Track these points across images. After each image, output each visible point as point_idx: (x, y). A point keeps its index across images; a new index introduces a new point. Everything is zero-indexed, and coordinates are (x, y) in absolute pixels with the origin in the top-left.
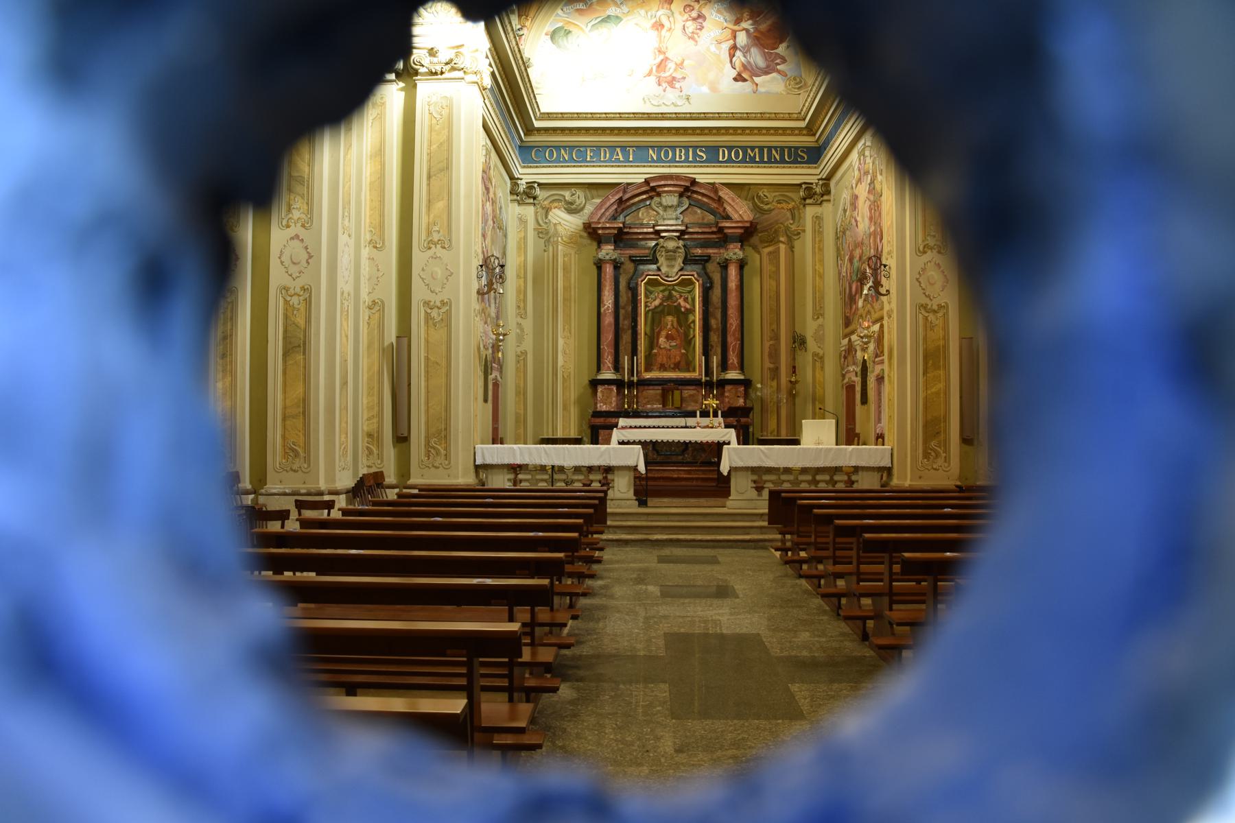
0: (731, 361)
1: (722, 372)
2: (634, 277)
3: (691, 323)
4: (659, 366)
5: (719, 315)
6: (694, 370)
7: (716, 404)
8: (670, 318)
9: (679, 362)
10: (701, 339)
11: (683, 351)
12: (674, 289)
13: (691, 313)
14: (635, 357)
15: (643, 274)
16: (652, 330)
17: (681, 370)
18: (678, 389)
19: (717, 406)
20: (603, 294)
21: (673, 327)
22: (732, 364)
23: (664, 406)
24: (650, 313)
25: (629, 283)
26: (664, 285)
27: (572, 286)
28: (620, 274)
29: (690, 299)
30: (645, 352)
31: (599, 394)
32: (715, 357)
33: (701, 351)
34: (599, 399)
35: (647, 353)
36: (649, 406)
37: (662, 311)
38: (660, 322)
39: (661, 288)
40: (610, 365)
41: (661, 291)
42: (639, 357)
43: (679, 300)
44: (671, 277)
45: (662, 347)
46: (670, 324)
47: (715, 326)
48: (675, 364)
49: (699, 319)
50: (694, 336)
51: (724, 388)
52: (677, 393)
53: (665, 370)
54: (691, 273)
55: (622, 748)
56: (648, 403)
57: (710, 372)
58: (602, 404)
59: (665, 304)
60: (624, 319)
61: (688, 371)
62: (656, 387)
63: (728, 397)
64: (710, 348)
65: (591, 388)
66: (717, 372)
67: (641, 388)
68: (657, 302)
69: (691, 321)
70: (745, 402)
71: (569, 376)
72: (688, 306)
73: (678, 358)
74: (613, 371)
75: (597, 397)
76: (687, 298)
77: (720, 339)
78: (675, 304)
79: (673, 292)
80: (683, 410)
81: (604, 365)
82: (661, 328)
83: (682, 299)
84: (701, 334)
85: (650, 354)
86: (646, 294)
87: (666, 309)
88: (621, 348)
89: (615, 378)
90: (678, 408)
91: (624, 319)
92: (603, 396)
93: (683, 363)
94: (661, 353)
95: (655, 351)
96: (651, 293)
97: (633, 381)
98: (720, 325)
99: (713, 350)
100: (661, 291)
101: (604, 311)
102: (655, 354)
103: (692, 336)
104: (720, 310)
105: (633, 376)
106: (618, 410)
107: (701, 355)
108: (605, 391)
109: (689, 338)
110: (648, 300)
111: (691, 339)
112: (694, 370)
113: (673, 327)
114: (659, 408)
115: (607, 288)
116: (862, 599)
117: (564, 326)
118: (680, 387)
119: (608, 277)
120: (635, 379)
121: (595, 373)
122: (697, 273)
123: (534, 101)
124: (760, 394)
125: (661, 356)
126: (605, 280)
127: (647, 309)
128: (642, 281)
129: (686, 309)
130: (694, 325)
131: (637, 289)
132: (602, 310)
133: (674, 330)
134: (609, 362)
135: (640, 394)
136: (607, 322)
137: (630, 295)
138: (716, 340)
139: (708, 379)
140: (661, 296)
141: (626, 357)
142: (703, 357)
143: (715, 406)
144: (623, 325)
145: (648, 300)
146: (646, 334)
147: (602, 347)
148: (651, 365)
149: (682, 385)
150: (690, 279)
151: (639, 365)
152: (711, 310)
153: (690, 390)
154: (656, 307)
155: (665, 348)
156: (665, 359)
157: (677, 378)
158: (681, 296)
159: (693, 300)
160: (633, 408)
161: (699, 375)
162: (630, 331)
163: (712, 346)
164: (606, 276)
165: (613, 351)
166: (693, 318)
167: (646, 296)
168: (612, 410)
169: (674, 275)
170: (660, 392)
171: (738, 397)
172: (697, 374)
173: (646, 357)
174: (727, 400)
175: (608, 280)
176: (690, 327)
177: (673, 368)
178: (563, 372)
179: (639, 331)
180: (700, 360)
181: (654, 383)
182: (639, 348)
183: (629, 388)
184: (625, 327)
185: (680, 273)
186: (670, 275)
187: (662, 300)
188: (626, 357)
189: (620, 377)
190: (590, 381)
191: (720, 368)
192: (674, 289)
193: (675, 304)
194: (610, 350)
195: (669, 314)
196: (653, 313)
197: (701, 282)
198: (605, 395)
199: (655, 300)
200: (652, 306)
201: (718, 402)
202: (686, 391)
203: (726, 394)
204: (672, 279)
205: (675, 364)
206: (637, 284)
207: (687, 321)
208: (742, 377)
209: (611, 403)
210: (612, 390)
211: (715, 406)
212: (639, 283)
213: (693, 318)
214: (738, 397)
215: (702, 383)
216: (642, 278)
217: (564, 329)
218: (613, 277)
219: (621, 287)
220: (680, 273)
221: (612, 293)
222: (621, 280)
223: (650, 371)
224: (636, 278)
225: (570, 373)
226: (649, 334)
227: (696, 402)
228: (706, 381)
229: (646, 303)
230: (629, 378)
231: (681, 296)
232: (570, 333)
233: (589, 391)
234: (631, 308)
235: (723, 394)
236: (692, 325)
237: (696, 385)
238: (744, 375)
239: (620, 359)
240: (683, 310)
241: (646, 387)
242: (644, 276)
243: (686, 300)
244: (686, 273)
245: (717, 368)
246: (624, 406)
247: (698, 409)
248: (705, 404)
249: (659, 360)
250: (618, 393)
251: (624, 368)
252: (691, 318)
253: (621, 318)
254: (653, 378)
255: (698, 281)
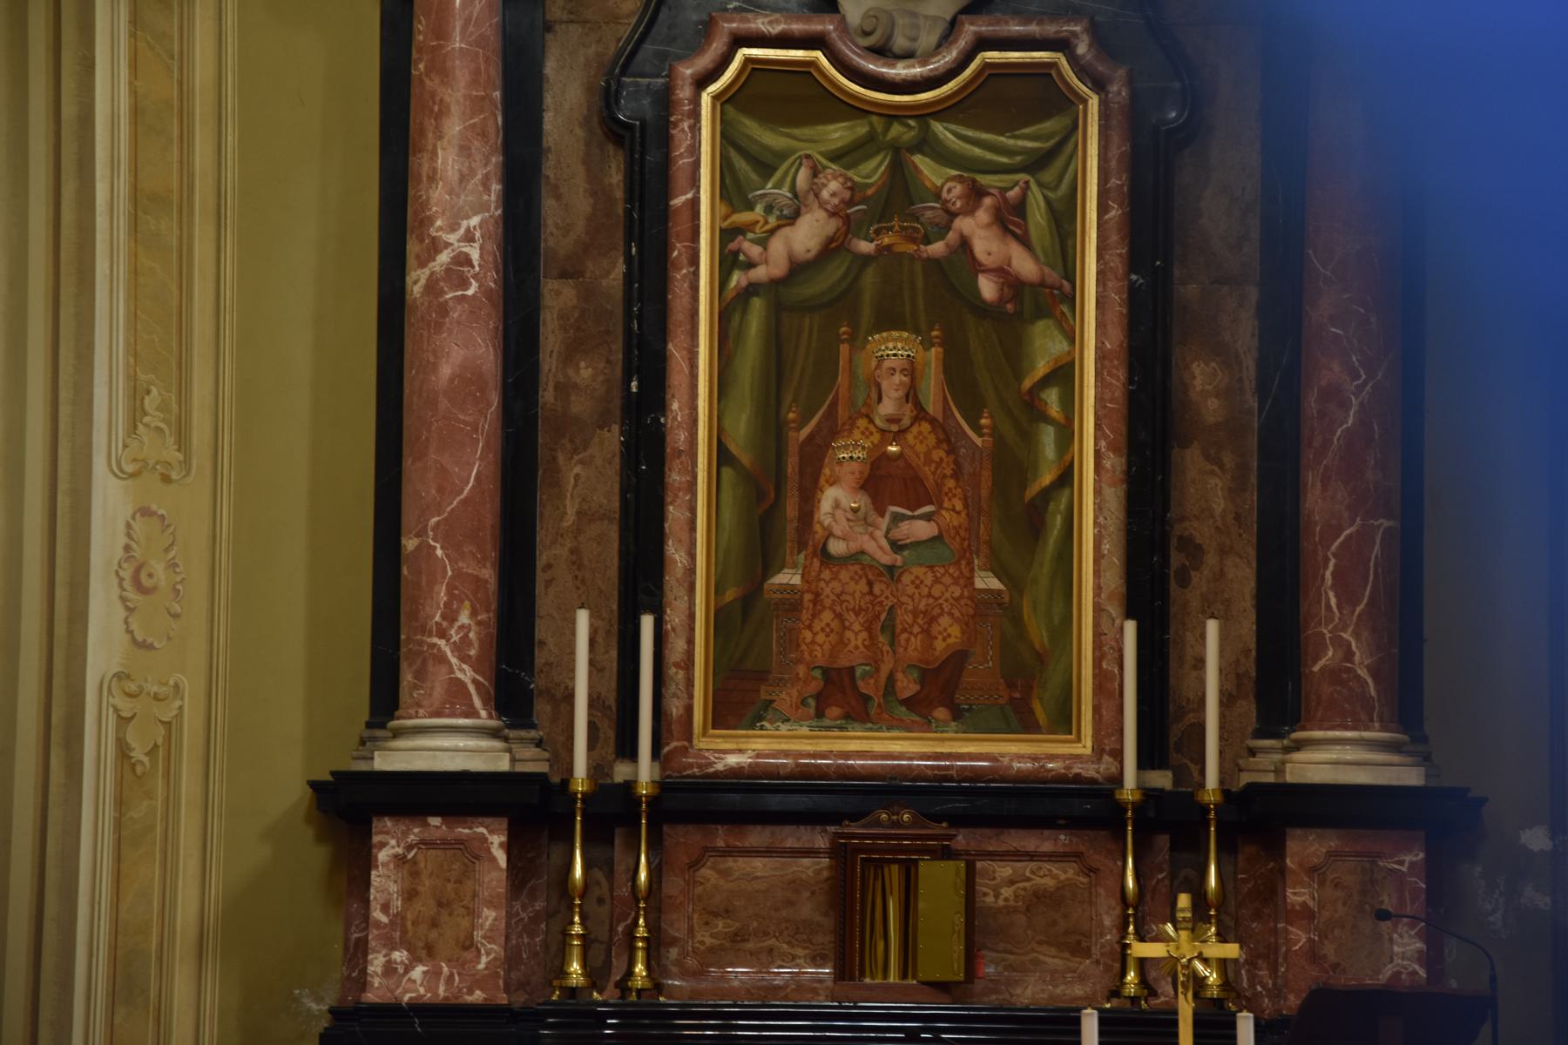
0: (1329, 656)
1: (1260, 734)
2: (648, 48)
3: (1046, 382)
4: (816, 686)
5: (1244, 334)
6: (1064, 721)
7: (1223, 964)
8: (894, 347)
9: (958, 659)
10: (1115, 498)
11: (987, 581)
12: (926, 144)
13: (1041, 313)
14: (647, 623)
15: (707, 28)
16: (771, 428)
17: (965, 718)
18: (947, 854)
19: (1226, 984)
20: (420, 164)
21: (920, 414)
22: (1336, 675)
23: (844, 972)
24: (757, 304)
25: (607, 97)
26: (858, 110)
27: (202, 106)
28: (548, 27)
29: (1038, 216)
30: (718, 587)
31: (384, 883)
32: (1212, 627)
33: (1114, 579)
34: (378, 915)
35: (730, 595)
36: (740, 972)
37: (842, 303)
38: (826, 369)
39: (838, 134)
40: (466, 674)
41: (836, 157)
42: (674, 617)
43: (964, 224)
44: (908, 55)
45: (837, 547)
46: (893, 387)
47: (1212, 409)
48: (927, 675)
49: (1101, 357)
50: (1066, 477)
51: (1275, 848)
52: (939, 879)
53: (859, 713)
54: (1051, 29)
55: (674, 965)
56: (735, 945)
57: (1175, 731)
58: (399, 956)
59: (865, 247)
60: (570, 355)
61: (1025, 724)
62: (792, 837)
63: (1307, 914)
64: (1176, 559)
65: (320, 838)
66: (1223, 738)
67: (682, 838)
68: (807, 235)
69: (1042, 368)
70: (1432, 958)
71: (165, 753)
72: (1025, 265)
73: (950, 633)
74: (484, 718)
75: (366, 902)
76: (1020, 208)
77: (1251, 499)
78: (937, 248)
79: (924, 164)
80: (985, 1002)
81: (421, 675)
82: (832, 413)
83: (982, 215)
84: (1115, 462)
85: (752, 594)
86: (725, 171)
87: (870, 278)
88: (550, 553)
89: (503, 765)
90: (942, 987)
91: (570, 355)
92: (410, 895)
93: (984, 667)
94: (828, 591)
95: (789, 577)
96: (765, 166)
97: (629, 786)
98: (1253, 402)
99: (1200, 580)
100: (836, 157)
101: (432, 287)
102: (791, 604)
103: (1047, 479)
104: (1253, 294)
105: (628, 750)
106: (520, 999)
107: (1114, 610)
108: (428, 861)
109: (1033, 490)
110: (743, 217)
111: (1047, 494)
112: (1064, 721)
113: (920, 414)
114: (812, 987)
115: (454, 127)
116: (936, 532)
117: (136, 394)
118: (962, 839)
119: (457, 43)
120: (645, 772)
121: (359, 728)
122: (1094, 31)
123: (1059, 859)
124: (1544, 902)
125: (827, 616)
126: (441, 70)
127: (737, 279)
128: (702, 82)
129: (1013, 285)
130: (1069, 401)
131: (666, 141)
132: (417, 281)
133: (921, 440)
134: (460, 649)
135: (673, 885)
136: (446, 370)
137: (615, 177)
138: (1219, 505)
139: (1162, 780)
140: (832, 187)
141: (583, 619)
142: (1130, 628)
143: (1213, 977)
144: (563, 389)
145: (743, 217)
146: (723, 455)
147: (409, 544)
148: (762, 676)
149: (960, 821)
150: (1044, 72)
151: (675, 674)
152: (1188, 291)
153: (1031, 856)
154: (798, 269)
155: (856, 557)
156: (857, 638)
157: (942, 776)
158: (976, 194)
159: (1064, 218)
160: (623, 986)
161: (1098, 750)
162: (613, 438)
163: (1194, 551)
164: (441, 33)
165: (488, 574)
166: (1058, 346)
167: (731, 191)
168: (478, 996)
169: (928, 39)
170: (813, 868)
171: (1383, 915)
172: (1085, 747)
173: (722, 622)
174: (1300, 937)
175: (461, 74)
176: (1038, 414)
177: (909, 703)
178: (123, 721)
179: (678, 438)
180: (1107, 649)
181: (774, 802)
182: (675, 554)
183: (598, 836)
184: (580, 406)
185: (971, 29)
186: (900, 43)
187: (848, 222)
188: (583, 619)
189: (533, 762)
190: (315, 786)
191: (1248, 708)
192: (926, 144)
193: (937, 248)
194: (469, 568)
195: (888, 320)
196: (778, 310)
197: (1118, 90)
198: (426, 884)
199: (792, 218)
200: (773, 261)
201: (1232, 950)
202: (1005, 870)
203: (1297, 895)
204: (917, 70)
205: (927, 675)
206: (665, 101)
207: (1019, 377)
208: (1411, 777)
209: (468, 944)
210: (475, 853)
211: (1213, 977)
212: (684, 93)
213: (1058, 346)
214: (1383, 915)
215: (1120, 807)
216: (705, 61)
217: (136, 415)
218: (495, 41)
219: (552, 123)
220: (971, 29)
221: (488, 165)
222: (550, 67)
223: (754, 722)
224: (663, 57)
225: (171, 728)
226: (745, 459)
227: (1077, 946)
228: (1150, 795)
229: (727, 235)
230: (597, 770)
231: (976, 194)
232: (183, 442)
233: (315, 856)
234: (621, 267)
235: (1268, 893)
236: (1052, 397)
237: (1075, 823)
238: (1425, 759)
239: (542, 630)
240: (987, 288)
241: (721, 837)
242: (717, 47)
243: (1010, 219)
244: (1015, 28)
245: (1226, 701)
246: (563, 973)
247: (1090, 1002)
248: (1142, 963)
249: (817, 639)
250: (520, 874)
251: (570, 697)
252: (1045, 347)
253: (551, 338)
254: (772, 773)
255: (1099, 85)
